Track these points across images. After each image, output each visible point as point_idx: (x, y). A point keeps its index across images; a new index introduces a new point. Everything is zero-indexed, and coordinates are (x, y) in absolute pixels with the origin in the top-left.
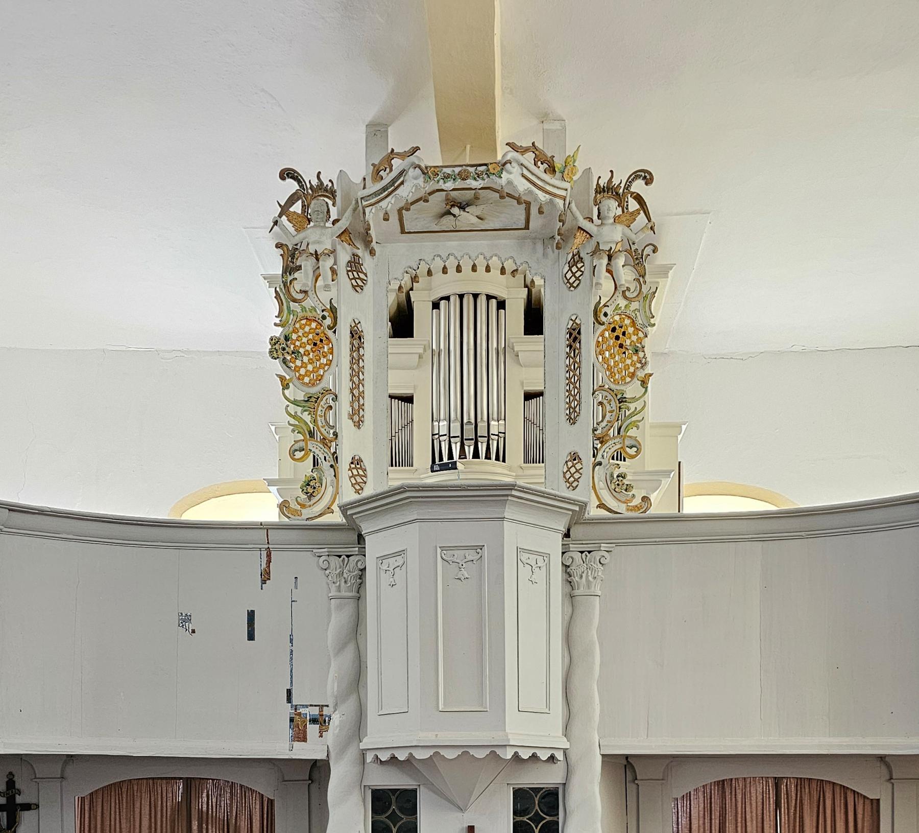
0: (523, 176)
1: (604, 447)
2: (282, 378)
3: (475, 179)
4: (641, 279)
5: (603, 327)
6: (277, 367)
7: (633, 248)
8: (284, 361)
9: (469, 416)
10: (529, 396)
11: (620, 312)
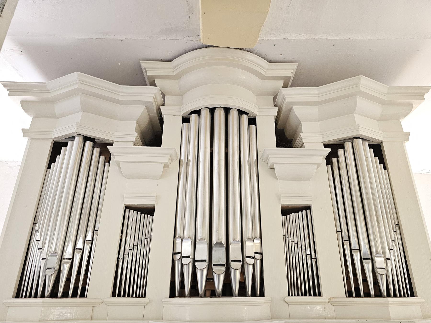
9: (219, 235)
10: (286, 211)
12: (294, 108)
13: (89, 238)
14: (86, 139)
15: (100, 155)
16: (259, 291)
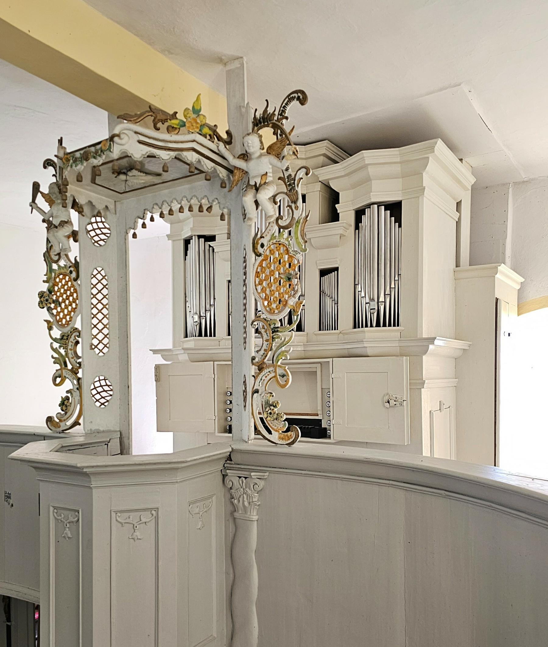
0: (140, 142)
1: (262, 374)
2: (48, 322)
3: (95, 158)
4: (293, 206)
5: (260, 258)
6: (44, 314)
7: (286, 175)
8: (49, 309)
11: (274, 241)
12: (330, 182)
13: (212, 303)
14: (200, 237)
15: (391, 216)
16: (213, 334)
